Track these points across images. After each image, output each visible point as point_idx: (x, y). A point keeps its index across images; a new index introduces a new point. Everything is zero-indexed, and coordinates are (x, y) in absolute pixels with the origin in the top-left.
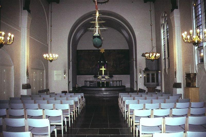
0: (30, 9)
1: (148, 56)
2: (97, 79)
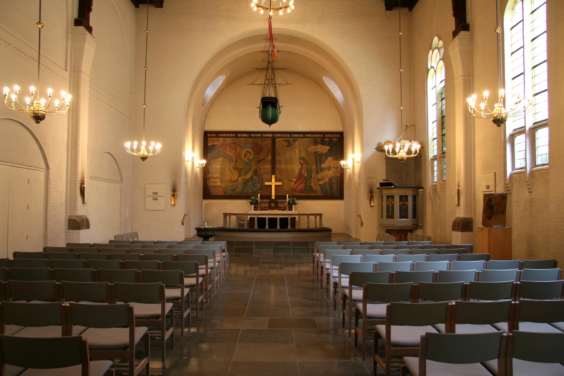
0: (91, 26)
1: (391, 151)
2: (175, 347)
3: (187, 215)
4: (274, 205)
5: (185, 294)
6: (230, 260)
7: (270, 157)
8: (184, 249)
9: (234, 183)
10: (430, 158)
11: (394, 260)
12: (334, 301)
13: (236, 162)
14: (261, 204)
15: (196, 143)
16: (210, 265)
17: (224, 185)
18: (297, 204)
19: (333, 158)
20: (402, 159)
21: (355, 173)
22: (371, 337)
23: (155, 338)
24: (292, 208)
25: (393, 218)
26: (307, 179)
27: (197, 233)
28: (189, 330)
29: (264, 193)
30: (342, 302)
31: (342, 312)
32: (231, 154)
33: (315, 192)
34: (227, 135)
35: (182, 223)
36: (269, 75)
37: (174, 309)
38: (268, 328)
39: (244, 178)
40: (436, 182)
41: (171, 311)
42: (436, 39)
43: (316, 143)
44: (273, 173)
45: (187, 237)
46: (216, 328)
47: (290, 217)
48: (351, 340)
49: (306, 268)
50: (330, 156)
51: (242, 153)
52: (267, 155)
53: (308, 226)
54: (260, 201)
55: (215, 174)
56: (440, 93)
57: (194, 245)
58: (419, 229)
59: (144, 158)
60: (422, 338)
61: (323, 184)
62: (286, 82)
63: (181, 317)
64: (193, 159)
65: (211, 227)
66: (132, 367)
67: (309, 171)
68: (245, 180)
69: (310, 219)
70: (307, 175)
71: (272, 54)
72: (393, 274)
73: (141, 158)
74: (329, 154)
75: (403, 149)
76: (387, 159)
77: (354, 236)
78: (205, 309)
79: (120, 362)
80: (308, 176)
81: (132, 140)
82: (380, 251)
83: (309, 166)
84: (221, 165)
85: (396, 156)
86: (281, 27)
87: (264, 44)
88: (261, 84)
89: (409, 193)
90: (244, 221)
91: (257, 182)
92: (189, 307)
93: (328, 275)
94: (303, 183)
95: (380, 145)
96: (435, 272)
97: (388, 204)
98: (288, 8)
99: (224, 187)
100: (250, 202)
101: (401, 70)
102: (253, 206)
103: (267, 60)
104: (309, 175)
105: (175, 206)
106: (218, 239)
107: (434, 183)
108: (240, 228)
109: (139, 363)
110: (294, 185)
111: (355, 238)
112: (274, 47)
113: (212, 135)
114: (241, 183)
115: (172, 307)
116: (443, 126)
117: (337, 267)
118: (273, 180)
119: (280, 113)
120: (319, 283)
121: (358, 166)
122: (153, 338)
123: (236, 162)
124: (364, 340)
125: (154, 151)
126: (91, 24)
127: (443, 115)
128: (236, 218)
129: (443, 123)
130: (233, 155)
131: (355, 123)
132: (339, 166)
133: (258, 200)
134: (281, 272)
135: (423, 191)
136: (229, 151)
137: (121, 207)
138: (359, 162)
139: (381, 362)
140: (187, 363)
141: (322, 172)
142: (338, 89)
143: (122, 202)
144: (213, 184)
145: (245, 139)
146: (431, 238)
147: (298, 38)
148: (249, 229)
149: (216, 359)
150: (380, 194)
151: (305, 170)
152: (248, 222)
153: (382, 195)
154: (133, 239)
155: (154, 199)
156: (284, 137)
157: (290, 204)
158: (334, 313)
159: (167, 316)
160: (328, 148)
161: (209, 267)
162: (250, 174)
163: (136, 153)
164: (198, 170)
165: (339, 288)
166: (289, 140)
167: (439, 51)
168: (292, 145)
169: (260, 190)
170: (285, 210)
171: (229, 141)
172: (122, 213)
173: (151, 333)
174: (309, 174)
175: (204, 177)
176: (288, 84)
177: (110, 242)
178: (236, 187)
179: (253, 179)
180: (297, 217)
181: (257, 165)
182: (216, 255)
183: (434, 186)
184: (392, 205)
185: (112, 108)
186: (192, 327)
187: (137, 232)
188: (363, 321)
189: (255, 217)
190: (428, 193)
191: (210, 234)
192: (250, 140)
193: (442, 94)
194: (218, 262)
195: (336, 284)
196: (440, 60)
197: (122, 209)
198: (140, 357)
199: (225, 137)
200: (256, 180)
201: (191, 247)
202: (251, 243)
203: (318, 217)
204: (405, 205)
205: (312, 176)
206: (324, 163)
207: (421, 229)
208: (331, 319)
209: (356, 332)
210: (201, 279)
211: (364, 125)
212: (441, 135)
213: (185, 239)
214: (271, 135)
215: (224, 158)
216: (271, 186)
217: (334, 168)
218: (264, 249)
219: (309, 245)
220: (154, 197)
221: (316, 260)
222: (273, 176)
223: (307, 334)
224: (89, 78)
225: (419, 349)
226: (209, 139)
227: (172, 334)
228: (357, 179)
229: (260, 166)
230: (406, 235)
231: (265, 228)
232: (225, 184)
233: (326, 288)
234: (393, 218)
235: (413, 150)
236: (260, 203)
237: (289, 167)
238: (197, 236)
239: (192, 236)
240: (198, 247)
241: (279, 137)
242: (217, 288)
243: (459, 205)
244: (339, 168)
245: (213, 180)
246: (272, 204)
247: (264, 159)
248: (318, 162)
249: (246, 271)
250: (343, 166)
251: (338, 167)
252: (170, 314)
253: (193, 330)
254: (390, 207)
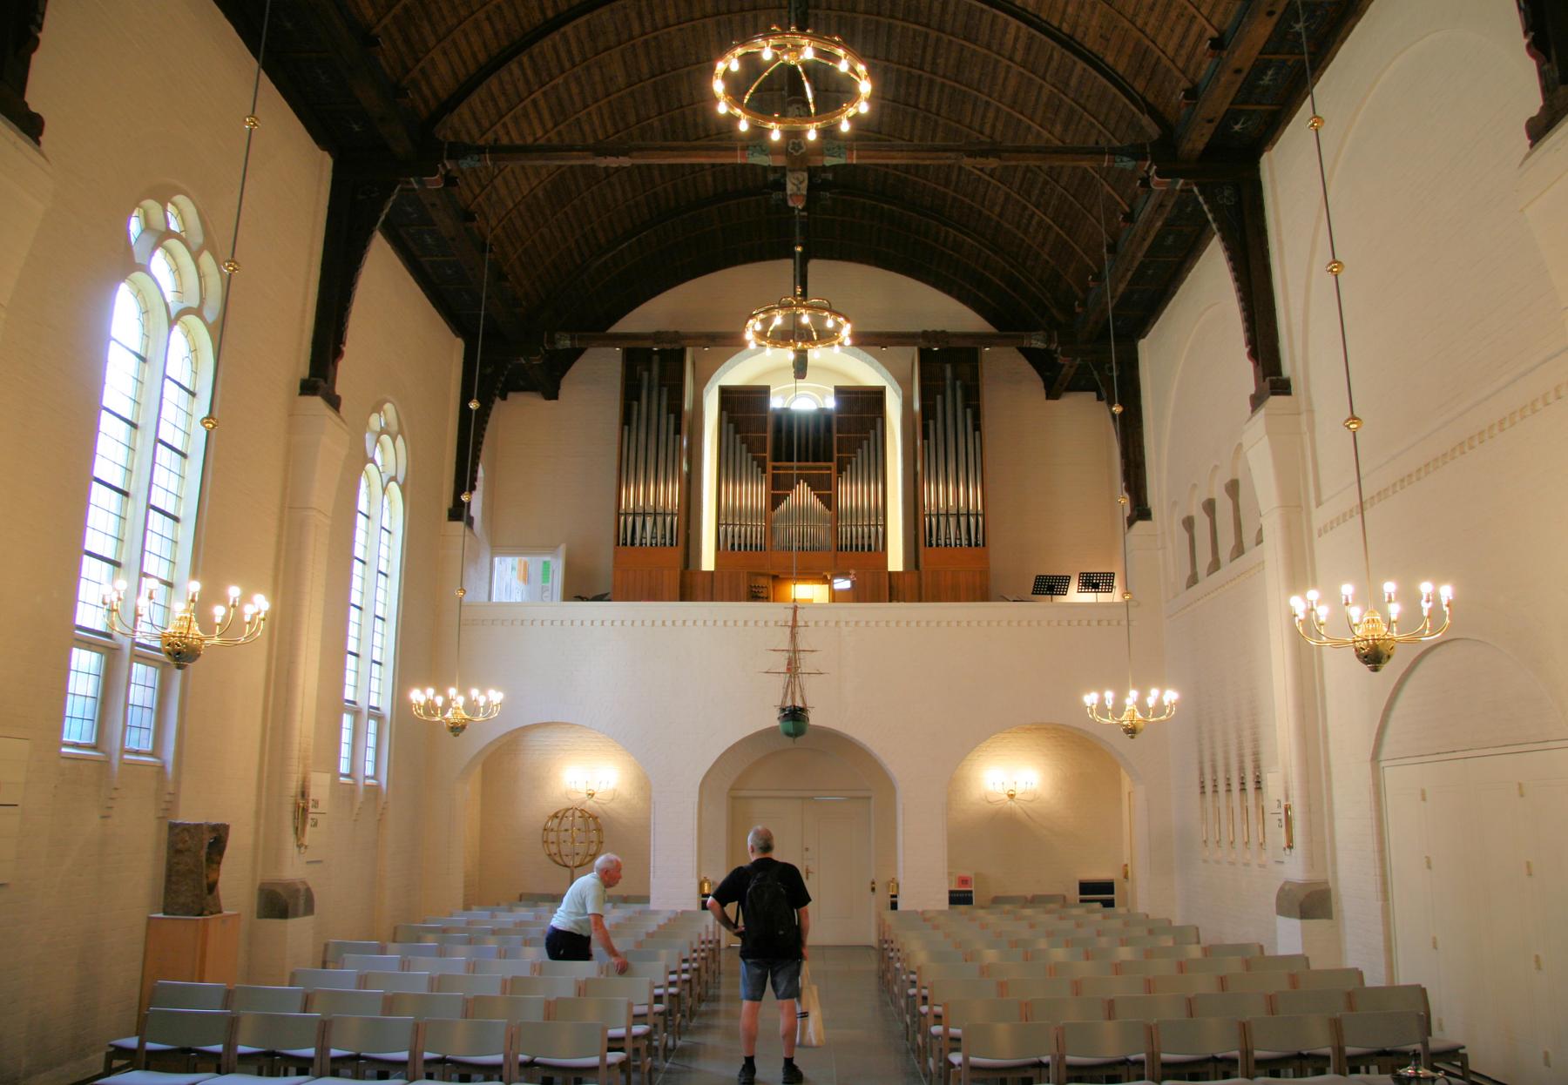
126: (339, 390)
223: (987, 349)
243: (1290, 847)
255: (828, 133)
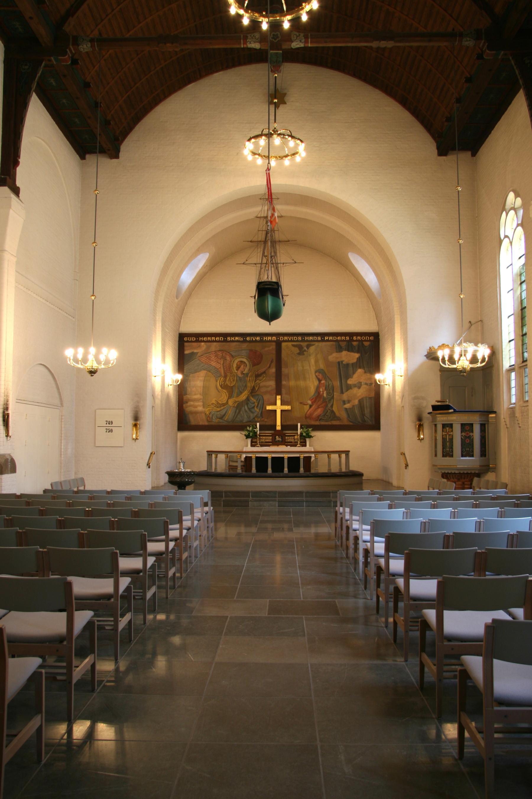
1: (447, 358)
3: (154, 454)
4: (280, 439)
5: (149, 564)
6: (215, 517)
7: (273, 370)
8: (149, 501)
9: (222, 408)
10: (504, 369)
11: (452, 516)
12: (364, 576)
13: (225, 377)
14: (261, 438)
15: (168, 350)
16: (187, 524)
17: (207, 411)
18: (312, 437)
19: (365, 371)
20: (464, 370)
21: (396, 391)
22: (417, 628)
23: (104, 629)
24: (305, 442)
25: (452, 456)
26: (327, 400)
27: (169, 478)
28: (155, 617)
29: (266, 421)
30: (375, 577)
31: (375, 592)
32: (218, 366)
33: (339, 419)
34: (211, 339)
35: (147, 465)
36: (268, 249)
37: (132, 586)
38: (269, 614)
39: (237, 400)
40: (514, 404)
41: (128, 589)
42: (511, 196)
43: (339, 349)
44: (278, 392)
45: (155, 485)
46: (193, 614)
47: (302, 456)
48: (389, 633)
49: (326, 530)
50: (360, 368)
51: (233, 363)
52: (269, 367)
53: (329, 469)
54: (260, 433)
55: (195, 395)
56: (519, 274)
57: (163, 495)
58: (489, 473)
59: (92, 372)
60: (488, 627)
61: (350, 409)
62: (293, 260)
63: (143, 598)
64: (163, 372)
65: (189, 470)
66: (70, 668)
67: (330, 390)
68: (237, 403)
69: (331, 459)
70: (326, 395)
71: (272, 220)
72: (448, 536)
73: (88, 372)
74: (359, 364)
75: (465, 355)
76: (443, 370)
77: (395, 483)
78: (179, 587)
79: (55, 661)
80: (329, 396)
81: (76, 346)
82: (431, 504)
83: (330, 382)
84: (204, 381)
85: (454, 366)
86: (288, 183)
87: (259, 208)
88: (256, 263)
89: (475, 420)
90: (237, 462)
91: (255, 406)
92: (154, 584)
93: (356, 538)
94: (322, 407)
95: (431, 350)
96: (511, 533)
97: (444, 437)
98: (297, 156)
99: (208, 413)
100: (245, 435)
101: (461, 241)
102: (249, 440)
103: (264, 229)
104: (330, 395)
105: (137, 440)
106: (199, 487)
107: (511, 404)
108: (231, 472)
109: (82, 662)
110: (308, 410)
111: (397, 486)
112: (274, 210)
113: (190, 339)
114: (232, 407)
115: (130, 583)
116: (524, 321)
117: (368, 527)
118: (279, 402)
119: (284, 305)
120: (344, 550)
121: (400, 383)
122: (100, 628)
123: (225, 377)
124: (406, 632)
125: (107, 362)
126: (18, 184)
127: (524, 306)
128: (226, 458)
129: (523, 318)
130: (220, 367)
131: (396, 319)
132: (373, 382)
133: (257, 431)
134: (289, 535)
135: (495, 417)
136: (215, 362)
137: (61, 443)
138: (401, 376)
139: (431, 664)
140: (151, 663)
141: (349, 391)
142: (371, 270)
143: (63, 435)
144: (193, 409)
145: (237, 343)
146: (507, 485)
147: (312, 198)
148: (244, 473)
149: (192, 659)
150: (432, 422)
151: (324, 388)
152: (243, 464)
153: (435, 423)
154: (78, 488)
155: (108, 431)
156: (294, 341)
157: (302, 438)
158: (365, 594)
159: (122, 596)
160: (357, 355)
161: (184, 526)
162: (245, 394)
163: (82, 364)
164: (170, 390)
165: (371, 557)
166: (301, 345)
167: (516, 213)
168: (304, 352)
169: (259, 417)
170: (295, 446)
171: (214, 346)
172: (63, 450)
173: (98, 621)
174: (330, 393)
175: (179, 398)
176: (295, 262)
177: (45, 491)
178: (226, 413)
179: (249, 402)
180: (313, 455)
181: (255, 382)
182: (195, 510)
183: (511, 409)
184: (451, 437)
185: (47, 301)
186: (158, 613)
187: (84, 477)
188: (405, 604)
189: (253, 456)
190: (502, 420)
191: (188, 481)
192: (245, 345)
193: (521, 275)
194: (198, 521)
195: (367, 552)
196: (518, 225)
197: (62, 444)
198: (82, 654)
199: (209, 341)
200: (254, 403)
201: (159, 498)
202: (246, 494)
203: (343, 456)
204: (469, 437)
205: (335, 396)
206: (352, 378)
207: (493, 473)
208: (361, 602)
209: (394, 621)
210: (172, 544)
211: (408, 322)
212: (521, 334)
213: (152, 488)
214: (274, 338)
215: (208, 372)
216: (276, 411)
217: (366, 384)
218: (266, 502)
219: (330, 497)
220: (107, 428)
221: (339, 516)
222: (279, 397)
224: (15, 259)
225: (482, 645)
226: (186, 344)
227: (130, 622)
228: (400, 400)
229: (260, 382)
230: (471, 481)
231: (267, 472)
232: (209, 409)
233: (353, 558)
234: (452, 456)
235: (480, 357)
236: (259, 436)
237: (302, 383)
238: (170, 485)
239: (162, 483)
240: (169, 498)
241: (286, 341)
242: (196, 557)
244: (373, 385)
245: (192, 403)
246: (277, 437)
247: (264, 372)
248: (342, 376)
249: (239, 534)
250: (379, 381)
251: (371, 384)
252: (126, 594)
253: (161, 617)
254: (448, 440)
255: (296, 22)
